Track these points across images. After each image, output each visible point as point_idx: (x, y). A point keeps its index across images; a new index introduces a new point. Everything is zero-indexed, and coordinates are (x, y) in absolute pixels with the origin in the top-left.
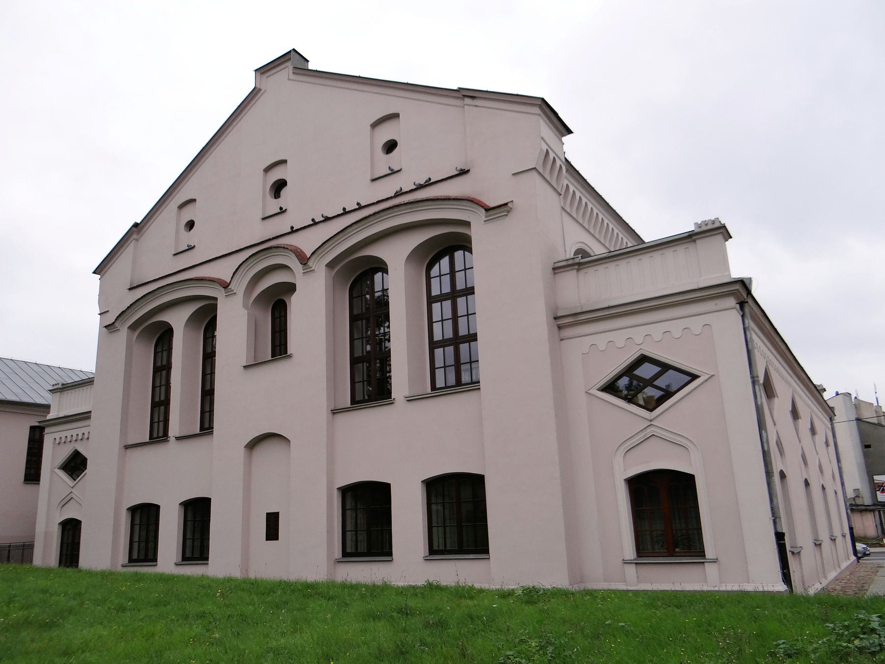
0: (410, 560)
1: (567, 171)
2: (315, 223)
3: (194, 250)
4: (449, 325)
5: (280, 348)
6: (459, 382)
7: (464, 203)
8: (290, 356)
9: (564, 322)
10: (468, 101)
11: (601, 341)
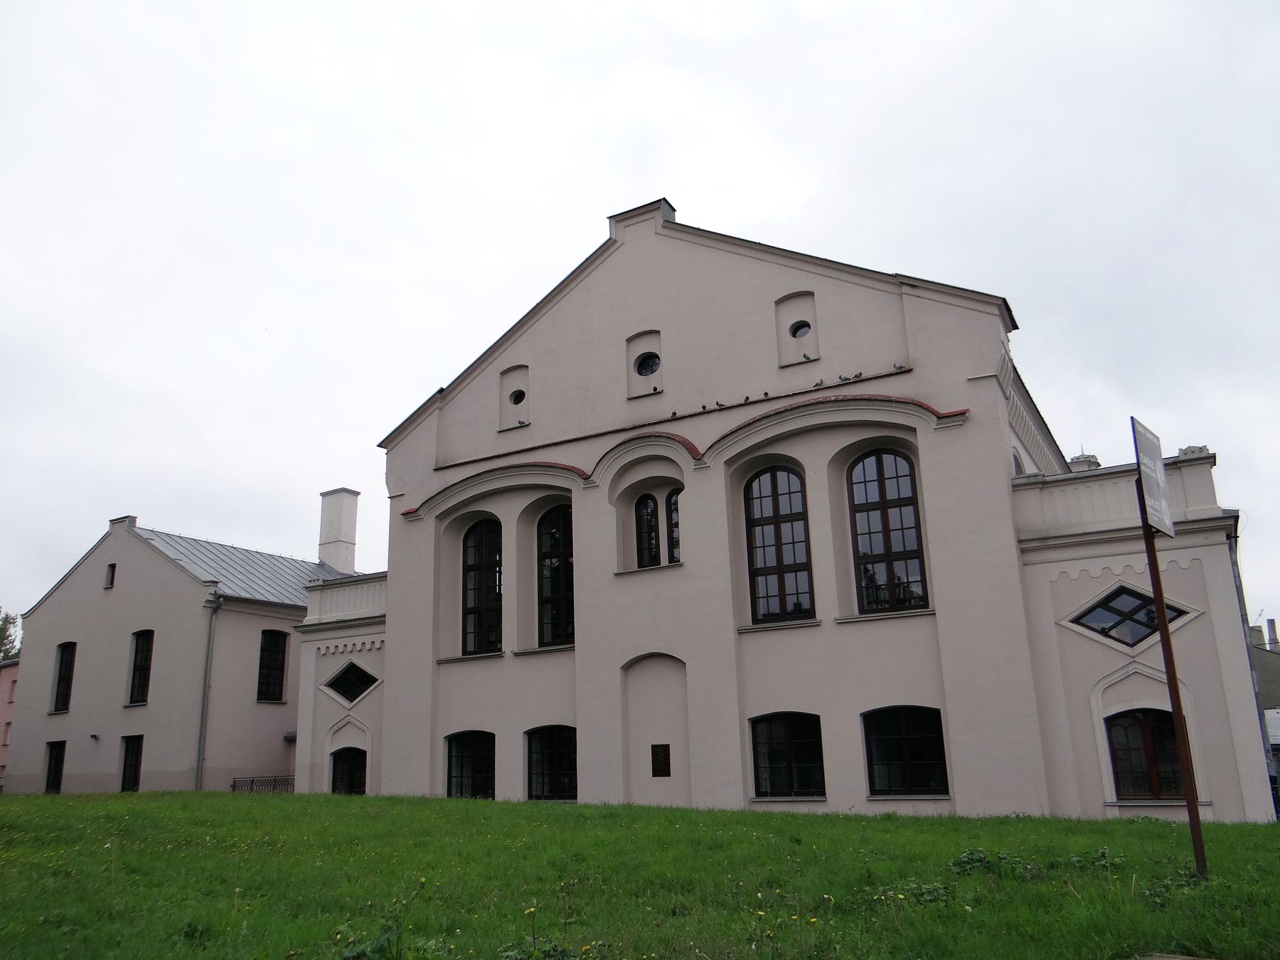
2: (705, 412)
3: (530, 428)
7: (910, 407)
8: (681, 565)
9: (1032, 545)
10: (905, 289)
11: (1074, 569)
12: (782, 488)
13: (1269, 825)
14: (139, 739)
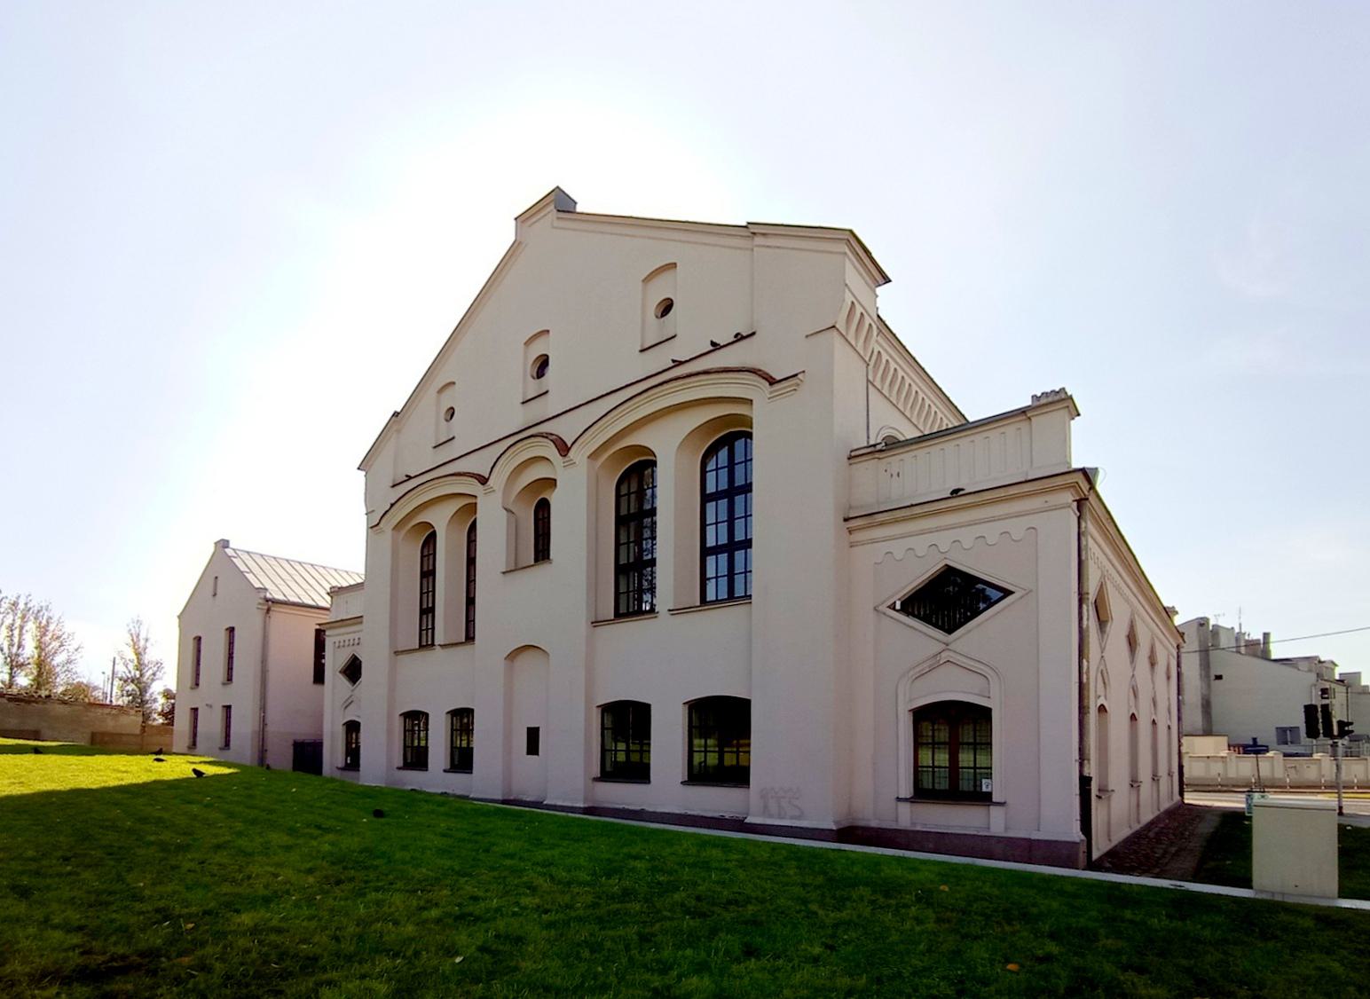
0: (667, 786)
1: (880, 331)
4: (723, 528)
5: (542, 552)
6: (731, 596)
9: (857, 520)
11: (898, 548)
13: (623, 762)
14: (468, 712)
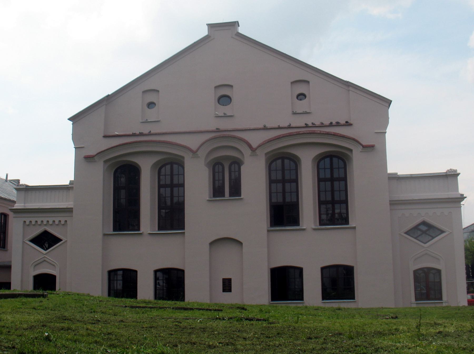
12: (335, 165)
